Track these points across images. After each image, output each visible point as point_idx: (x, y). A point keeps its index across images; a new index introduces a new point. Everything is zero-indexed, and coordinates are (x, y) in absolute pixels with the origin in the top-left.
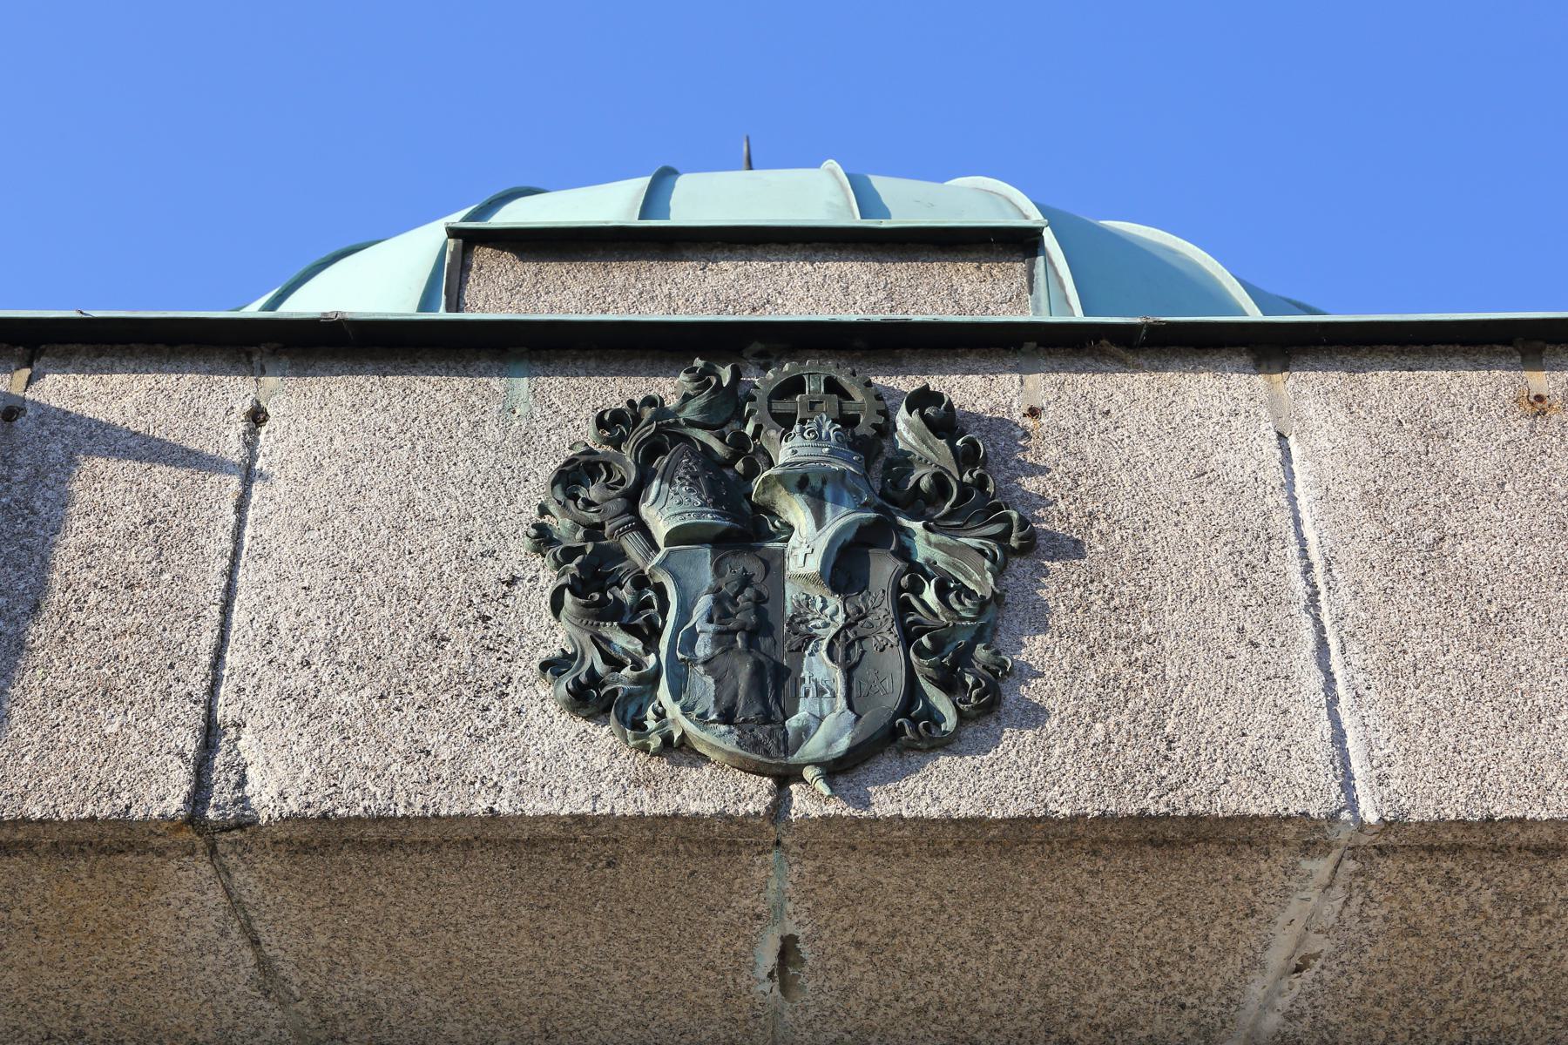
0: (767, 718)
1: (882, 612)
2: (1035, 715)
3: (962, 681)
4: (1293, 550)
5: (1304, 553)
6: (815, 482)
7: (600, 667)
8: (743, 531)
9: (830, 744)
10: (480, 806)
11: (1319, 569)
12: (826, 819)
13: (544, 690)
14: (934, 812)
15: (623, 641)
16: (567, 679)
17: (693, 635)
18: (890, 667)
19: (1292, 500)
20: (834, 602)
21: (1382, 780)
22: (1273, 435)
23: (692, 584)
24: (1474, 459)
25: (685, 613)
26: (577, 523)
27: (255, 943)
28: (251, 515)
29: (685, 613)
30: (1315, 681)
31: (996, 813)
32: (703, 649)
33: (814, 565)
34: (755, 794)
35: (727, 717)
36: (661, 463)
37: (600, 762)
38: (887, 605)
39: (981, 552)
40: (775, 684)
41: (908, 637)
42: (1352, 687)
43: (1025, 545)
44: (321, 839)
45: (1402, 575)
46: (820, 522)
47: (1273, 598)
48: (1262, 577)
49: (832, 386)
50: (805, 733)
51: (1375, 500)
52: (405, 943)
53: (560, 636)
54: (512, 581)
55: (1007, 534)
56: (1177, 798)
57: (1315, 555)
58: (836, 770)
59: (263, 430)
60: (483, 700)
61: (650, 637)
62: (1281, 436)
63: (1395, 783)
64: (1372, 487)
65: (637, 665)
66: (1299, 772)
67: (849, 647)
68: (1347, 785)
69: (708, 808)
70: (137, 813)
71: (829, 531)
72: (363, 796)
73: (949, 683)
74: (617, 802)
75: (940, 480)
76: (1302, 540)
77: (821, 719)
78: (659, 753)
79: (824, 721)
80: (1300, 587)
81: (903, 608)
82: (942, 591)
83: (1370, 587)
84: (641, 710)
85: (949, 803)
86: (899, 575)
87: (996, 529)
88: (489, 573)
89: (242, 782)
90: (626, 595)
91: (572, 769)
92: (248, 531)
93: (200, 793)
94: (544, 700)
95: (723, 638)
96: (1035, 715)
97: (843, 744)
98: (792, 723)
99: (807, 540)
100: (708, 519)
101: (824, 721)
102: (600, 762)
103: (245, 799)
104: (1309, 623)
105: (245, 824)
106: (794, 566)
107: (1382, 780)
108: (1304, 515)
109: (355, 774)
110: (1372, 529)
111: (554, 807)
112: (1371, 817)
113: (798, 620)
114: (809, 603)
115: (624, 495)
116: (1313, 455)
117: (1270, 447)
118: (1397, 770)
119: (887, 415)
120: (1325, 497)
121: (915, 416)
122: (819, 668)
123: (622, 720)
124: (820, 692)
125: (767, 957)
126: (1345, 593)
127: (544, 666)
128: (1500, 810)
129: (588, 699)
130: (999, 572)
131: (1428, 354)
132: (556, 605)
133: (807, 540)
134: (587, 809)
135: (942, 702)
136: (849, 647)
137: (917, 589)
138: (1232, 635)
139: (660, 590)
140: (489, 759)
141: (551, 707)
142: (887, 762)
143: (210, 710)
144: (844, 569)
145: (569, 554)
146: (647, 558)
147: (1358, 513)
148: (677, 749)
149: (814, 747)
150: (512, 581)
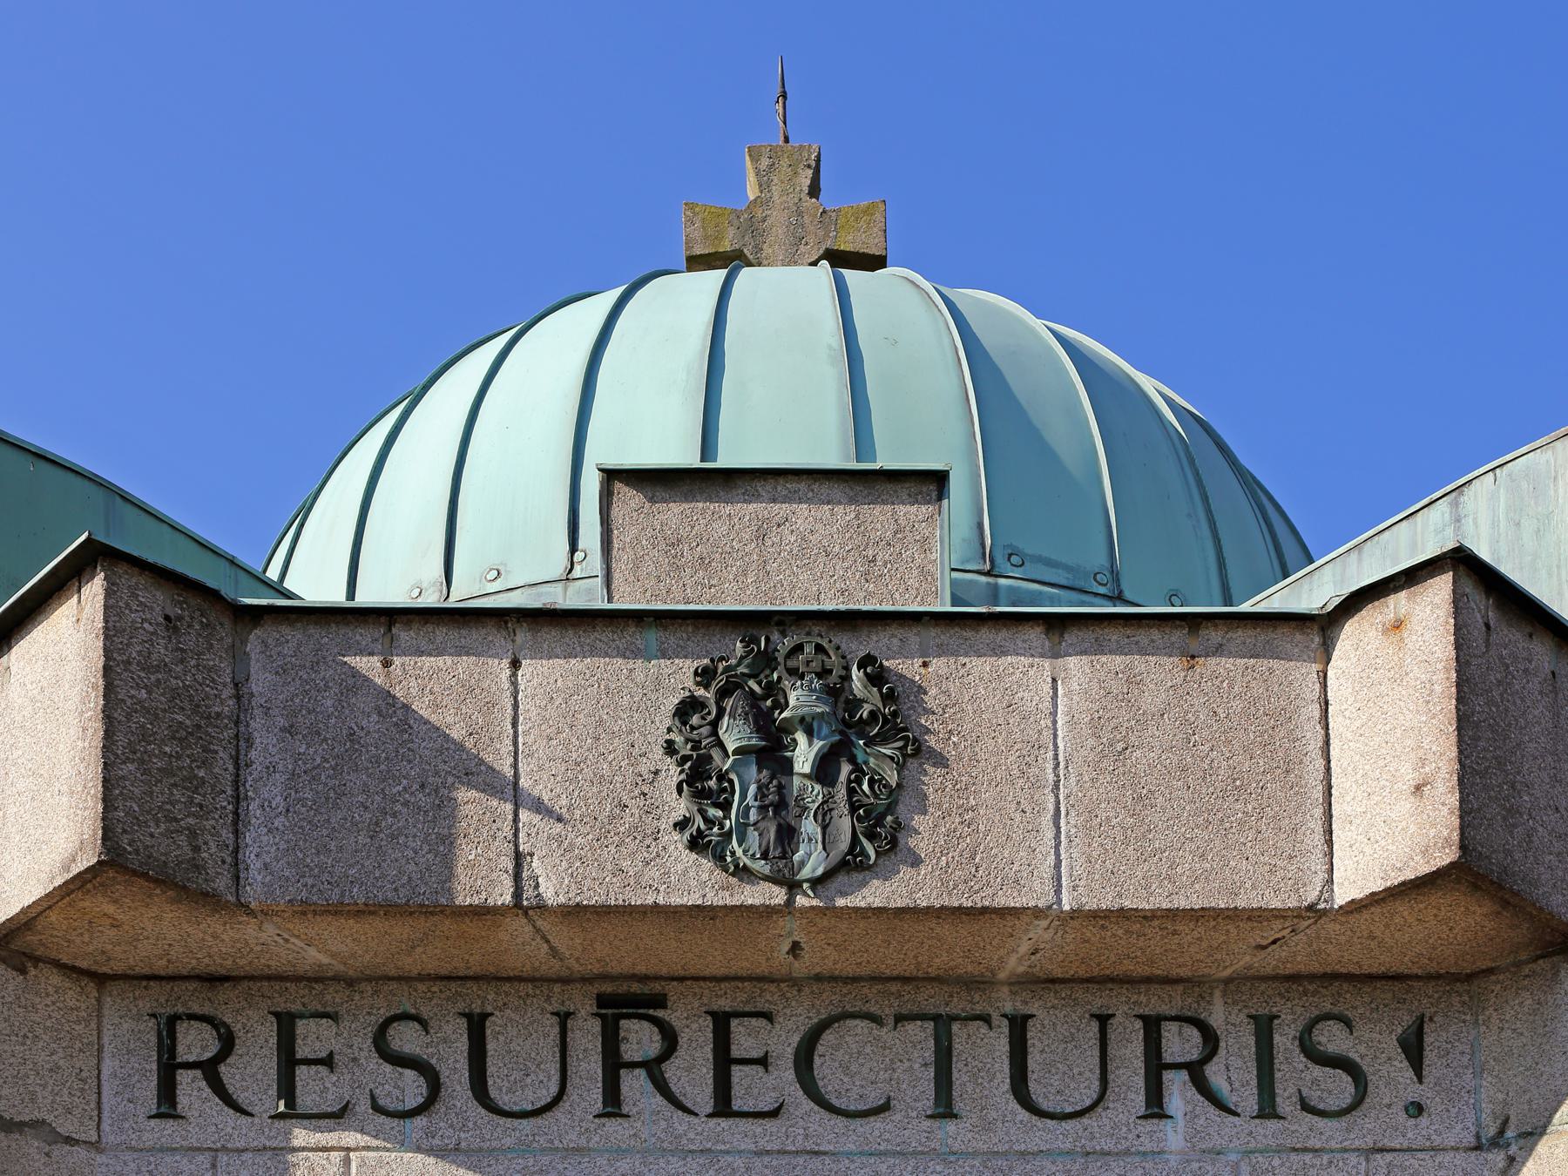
0: (784, 856)
1: (841, 792)
2: (916, 862)
3: (880, 833)
4: (1051, 754)
5: (1056, 755)
6: (808, 719)
7: (703, 827)
8: (771, 752)
9: (814, 871)
10: (650, 901)
11: (1062, 765)
12: (812, 907)
13: (676, 836)
14: (863, 904)
15: (714, 812)
16: (687, 835)
17: (748, 808)
18: (844, 825)
19: (1055, 722)
20: (818, 787)
21: (1075, 888)
22: (1049, 680)
23: (746, 777)
24: (1151, 700)
25: (744, 796)
26: (687, 740)
27: (548, 941)
28: (520, 729)
29: (744, 796)
30: (1050, 834)
31: (892, 905)
32: (753, 816)
33: (807, 769)
34: (778, 895)
35: (765, 856)
36: (729, 703)
37: (705, 877)
38: (844, 791)
39: (892, 758)
40: (788, 836)
41: (853, 809)
42: (1068, 836)
43: (915, 751)
44: (574, 913)
45: (1103, 771)
46: (810, 744)
47: (1036, 785)
48: (1034, 770)
49: (819, 649)
50: (802, 864)
51: (1096, 725)
52: (617, 942)
53: (682, 807)
54: (656, 773)
55: (905, 746)
56: (977, 898)
57: (1061, 758)
58: (816, 882)
59: (520, 673)
60: (647, 842)
61: (726, 806)
62: (1054, 680)
63: (1080, 889)
64: (1096, 715)
65: (722, 827)
66: (1037, 885)
67: (824, 815)
68: (1058, 892)
69: (757, 902)
70: (491, 902)
71: (816, 749)
72: (593, 896)
73: (872, 837)
74: (714, 899)
75: (873, 715)
76: (1056, 747)
77: (810, 855)
78: (733, 875)
79: (812, 860)
80: (1051, 777)
81: (851, 792)
82: (871, 782)
83: (1086, 778)
84: (723, 850)
85: (870, 900)
86: (851, 773)
87: (900, 744)
88: (645, 768)
89: (537, 886)
90: (712, 783)
91: (691, 881)
92: (520, 740)
93: (518, 894)
94: (676, 843)
95: (762, 809)
96: (916, 862)
97: (820, 871)
98: (796, 858)
99: (804, 755)
100: (754, 742)
101: (812, 860)
102: (705, 877)
103: (539, 895)
104: (1052, 800)
105: (541, 907)
106: (797, 768)
107: (1075, 888)
108: (1059, 733)
109: (588, 882)
110: (1091, 742)
111: (684, 901)
112: (1067, 908)
113: (800, 799)
114: (805, 789)
115: (710, 724)
116: (1069, 694)
117: (1047, 688)
118: (1082, 883)
119: (847, 668)
120: (1072, 722)
121: (861, 673)
122: (809, 826)
123: (714, 856)
124: (810, 840)
125: (786, 947)
126: (1073, 780)
127: (675, 825)
128: (1127, 904)
129: (696, 844)
130: (901, 768)
131: (1140, 627)
132: (680, 791)
133: (804, 755)
134: (699, 902)
135: (870, 850)
136: (824, 815)
137: (859, 781)
138: (1014, 806)
139: (731, 782)
140: (653, 873)
141: (680, 846)
142: (842, 879)
143: (516, 846)
144: (824, 771)
145: (685, 759)
146: (724, 763)
147: (1087, 731)
148: (742, 872)
149: (806, 873)
150: (656, 773)
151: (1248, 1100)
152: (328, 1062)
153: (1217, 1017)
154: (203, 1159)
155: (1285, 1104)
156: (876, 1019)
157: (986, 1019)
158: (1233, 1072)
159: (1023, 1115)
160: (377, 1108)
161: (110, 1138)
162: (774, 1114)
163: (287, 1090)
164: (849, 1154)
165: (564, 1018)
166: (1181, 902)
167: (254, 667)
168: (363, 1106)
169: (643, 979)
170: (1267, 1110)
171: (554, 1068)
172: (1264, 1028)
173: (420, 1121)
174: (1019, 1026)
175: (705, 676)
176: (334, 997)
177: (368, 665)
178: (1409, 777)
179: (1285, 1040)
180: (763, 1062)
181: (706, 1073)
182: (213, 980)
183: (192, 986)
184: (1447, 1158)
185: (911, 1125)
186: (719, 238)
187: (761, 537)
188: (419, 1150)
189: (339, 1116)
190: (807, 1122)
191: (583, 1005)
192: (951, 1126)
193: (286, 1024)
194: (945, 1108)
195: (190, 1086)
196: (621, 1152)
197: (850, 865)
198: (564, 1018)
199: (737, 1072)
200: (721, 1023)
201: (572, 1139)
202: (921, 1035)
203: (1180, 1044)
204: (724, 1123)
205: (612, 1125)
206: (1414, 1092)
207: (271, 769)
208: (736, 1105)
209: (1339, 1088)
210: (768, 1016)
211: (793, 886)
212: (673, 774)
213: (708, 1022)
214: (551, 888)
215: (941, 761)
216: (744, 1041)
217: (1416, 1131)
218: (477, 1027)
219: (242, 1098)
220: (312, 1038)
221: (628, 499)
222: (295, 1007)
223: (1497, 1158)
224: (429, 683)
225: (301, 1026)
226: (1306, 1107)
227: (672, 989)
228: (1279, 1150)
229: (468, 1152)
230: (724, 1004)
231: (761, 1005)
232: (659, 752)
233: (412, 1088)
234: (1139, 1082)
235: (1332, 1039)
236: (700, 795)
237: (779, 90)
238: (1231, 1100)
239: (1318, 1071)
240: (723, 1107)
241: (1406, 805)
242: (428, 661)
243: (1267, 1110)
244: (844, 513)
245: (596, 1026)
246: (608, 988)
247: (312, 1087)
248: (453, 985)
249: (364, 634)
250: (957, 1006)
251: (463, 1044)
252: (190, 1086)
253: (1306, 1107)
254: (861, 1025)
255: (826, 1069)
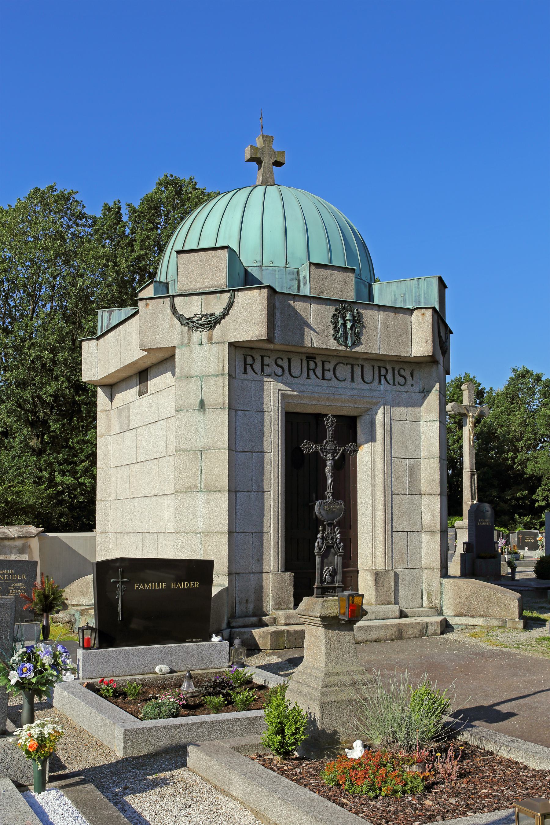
2: (362, 344)
3: (357, 341)
8: (344, 325)
47: (377, 333)
51: (384, 323)
61: (339, 333)
73: (357, 339)
74: (337, 348)
91: (333, 345)
99: (349, 325)
101: (349, 343)
122: (349, 337)
129: (335, 339)
133: (349, 325)
149: (349, 345)
151: (391, 382)
152: (268, 365)
153: (388, 367)
154: (250, 382)
155: (396, 384)
156: (344, 364)
157: (358, 365)
158: (390, 377)
159: (363, 382)
160: (275, 374)
161: (237, 377)
162: (330, 380)
163: (262, 371)
164: (340, 388)
165: (302, 360)
166: (394, 354)
167: (276, 301)
168: (273, 374)
169: (312, 354)
170: (394, 384)
171: (300, 369)
172: (393, 369)
173: (281, 377)
174: (362, 366)
175: (336, 310)
176: (269, 353)
177: (291, 302)
178: (425, 339)
179: (396, 372)
180: (329, 370)
181: (321, 371)
182: (252, 348)
183: (248, 349)
184: (416, 394)
185: (347, 383)
186: (256, 154)
187: (330, 276)
188: (281, 383)
189: (269, 376)
190: (335, 382)
191: (304, 358)
192: (353, 384)
193: (262, 357)
194: (353, 380)
195: (249, 368)
196: (309, 385)
197: (354, 345)
198: (302, 360)
199: (325, 372)
200: (323, 362)
201: (303, 382)
202: (349, 366)
203: (383, 372)
204: (323, 381)
205: (308, 380)
206: (412, 382)
207: (278, 320)
208: (325, 378)
209: (402, 381)
210: (330, 362)
211: (347, 347)
212: (332, 326)
213: (321, 362)
214: (316, 345)
215: (365, 328)
216: (326, 367)
217: (412, 389)
218: (289, 360)
219: (256, 371)
220: (267, 361)
221: (313, 267)
222: (263, 355)
223: (423, 395)
224: (299, 306)
225: (265, 358)
226: (399, 384)
227: (316, 356)
228: (395, 391)
229: (289, 383)
230: (323, 359)
231: (329, 360)
232: (330, 322)
233: (279, 371)
234: (378, 378)
235: (402, 372)
236: (335, 331)
237: (260, 116)
238: (390, 382)
239: (400, 378)
240: (323, 378)
241: (424, 344)
242: (300, 303)
243: (394, 384)
244: (341, 274)
245: (306, 362)
246: (307, 355)
247: (267, 370)
248: (286, 353)
249: (291, 297)
250: (354, 362)
251: (287, 364)
252: (249, 368)
253: (399, 384)
254: (342, 365)
255: (337, 372)
